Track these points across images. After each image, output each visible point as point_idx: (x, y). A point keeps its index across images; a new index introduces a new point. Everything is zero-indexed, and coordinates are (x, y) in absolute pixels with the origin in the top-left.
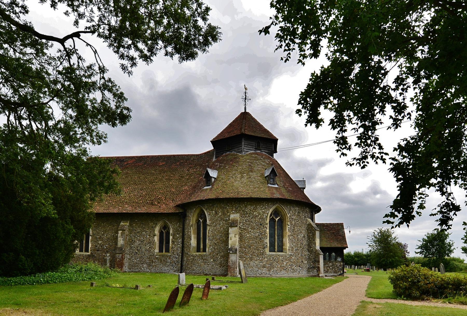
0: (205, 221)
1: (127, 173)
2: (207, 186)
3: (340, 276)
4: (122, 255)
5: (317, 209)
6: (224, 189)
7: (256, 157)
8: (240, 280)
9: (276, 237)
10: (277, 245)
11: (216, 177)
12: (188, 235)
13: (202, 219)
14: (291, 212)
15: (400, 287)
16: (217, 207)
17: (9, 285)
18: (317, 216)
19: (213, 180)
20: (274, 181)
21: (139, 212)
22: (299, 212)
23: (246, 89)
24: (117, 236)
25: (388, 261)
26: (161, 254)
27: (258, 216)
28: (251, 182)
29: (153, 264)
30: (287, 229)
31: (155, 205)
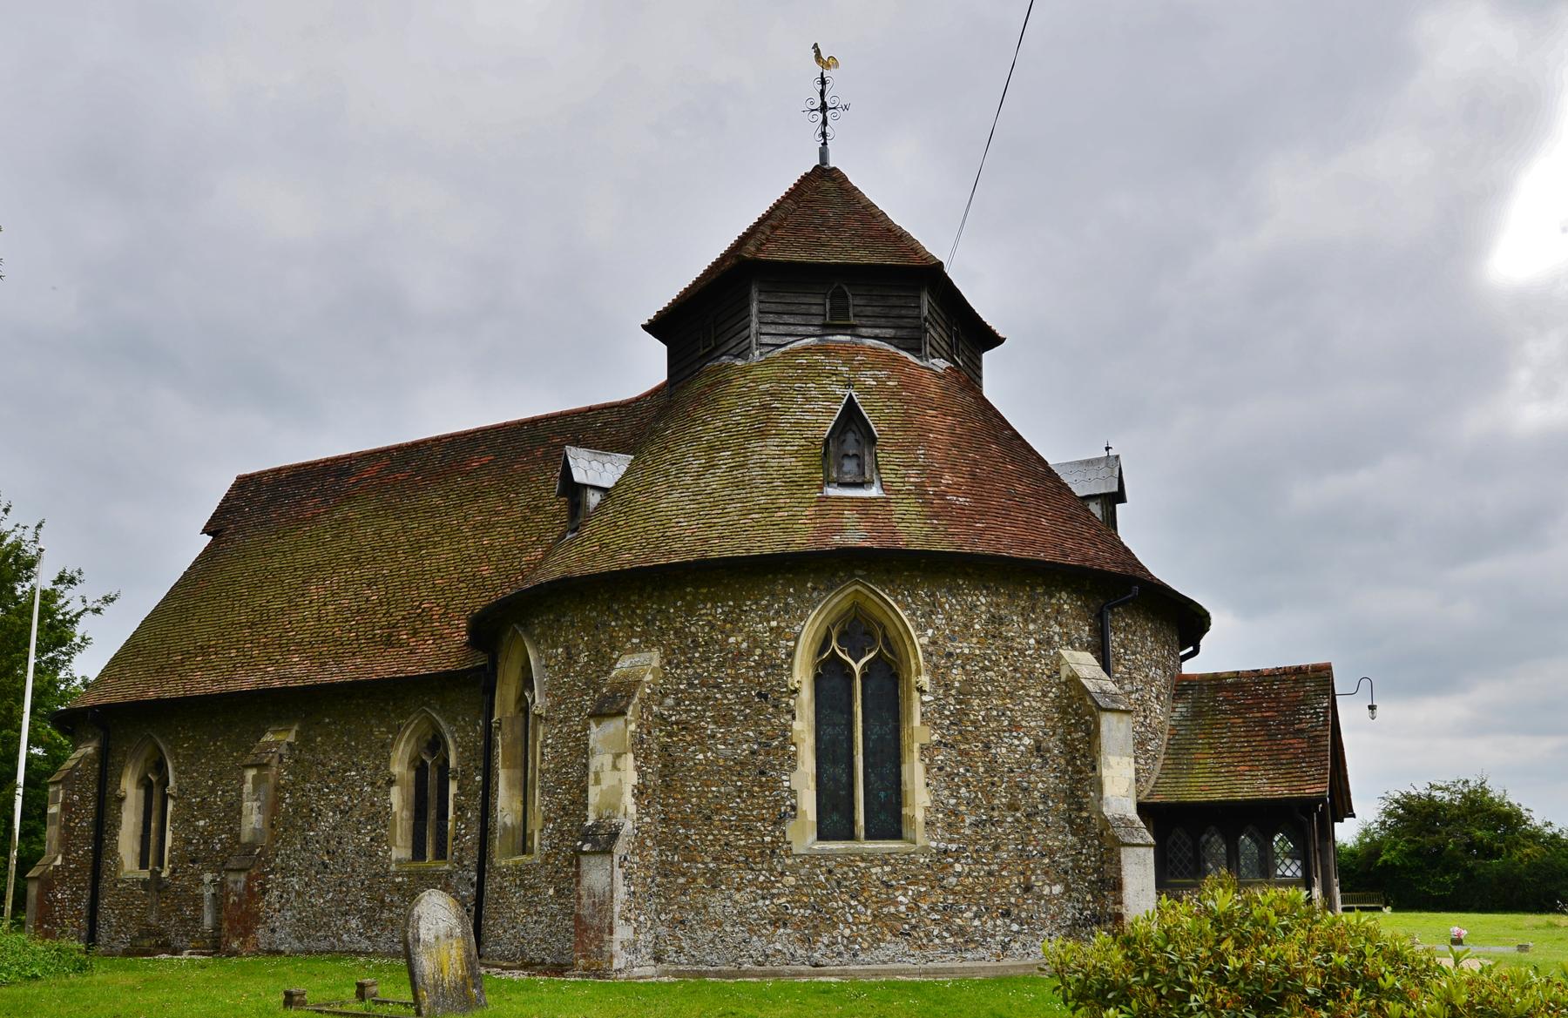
1: (345, 520)
10: (863, 795)
14: (939, 620)
19: (594, 499)
24: (240, 795)
27: (750, 652)
29: (385, 915)
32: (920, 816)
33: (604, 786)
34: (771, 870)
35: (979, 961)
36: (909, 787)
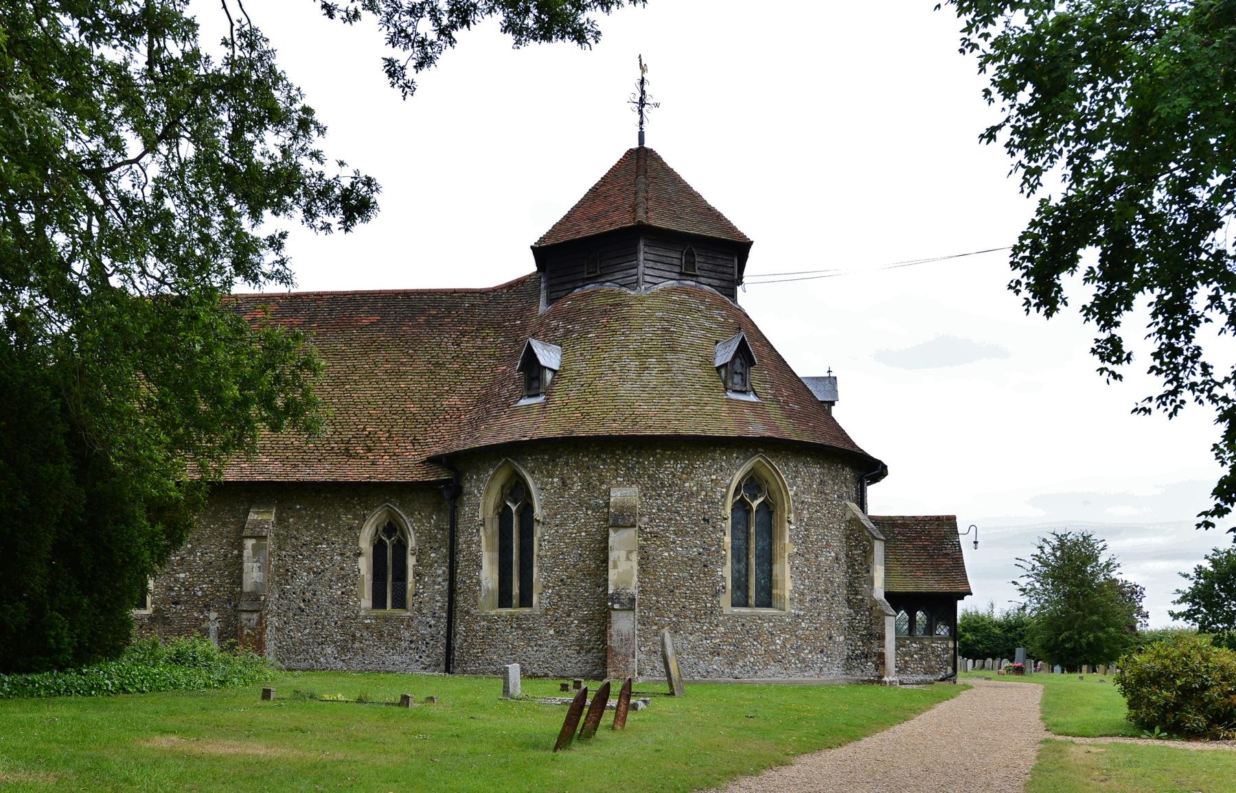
0: (527, 509)
2: (530, 396)
3: (946, 683)
4: (261, 617)
5: (873, 470)
6: (586, 409)
7: (682, 303)
8: (667, 690)
9: (753, 561)
11: (556, 368)
12: (471, 553)
13: (515, 502)
15: (1150, 704)
16: (567, 464)
17: (32, 696)
18: (874, 492)
19: (549, 376)
20: (744, 380)
21: (307, 478)
22: (822, 483)
23: (643, 68)
25: (1084, 641)
26: (380, 612)
28: (672, 384)
29: (357, 645)
30: (787, 533)
31: (356, 456)
32: (787, 595)
33: (620, 569)
34: (710, 623)
35: (810, 677)
36: (780, 578)
